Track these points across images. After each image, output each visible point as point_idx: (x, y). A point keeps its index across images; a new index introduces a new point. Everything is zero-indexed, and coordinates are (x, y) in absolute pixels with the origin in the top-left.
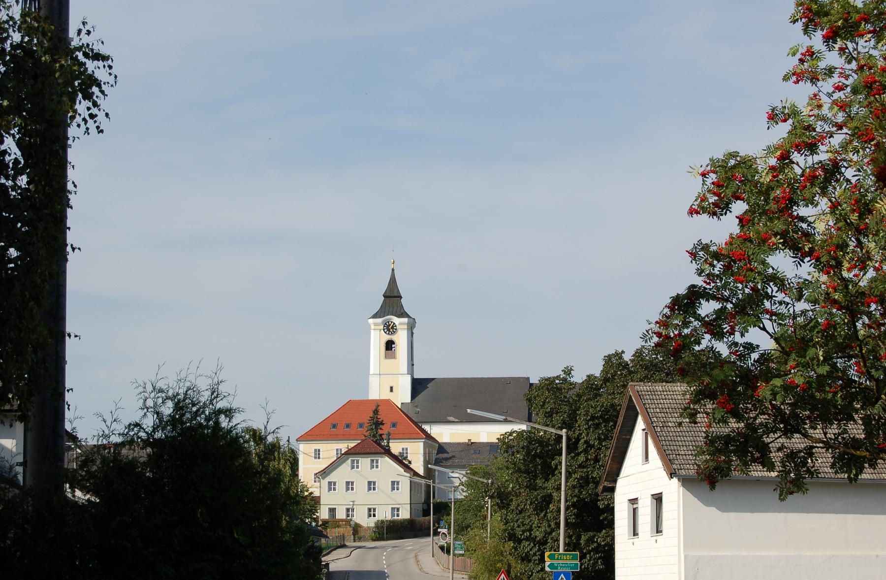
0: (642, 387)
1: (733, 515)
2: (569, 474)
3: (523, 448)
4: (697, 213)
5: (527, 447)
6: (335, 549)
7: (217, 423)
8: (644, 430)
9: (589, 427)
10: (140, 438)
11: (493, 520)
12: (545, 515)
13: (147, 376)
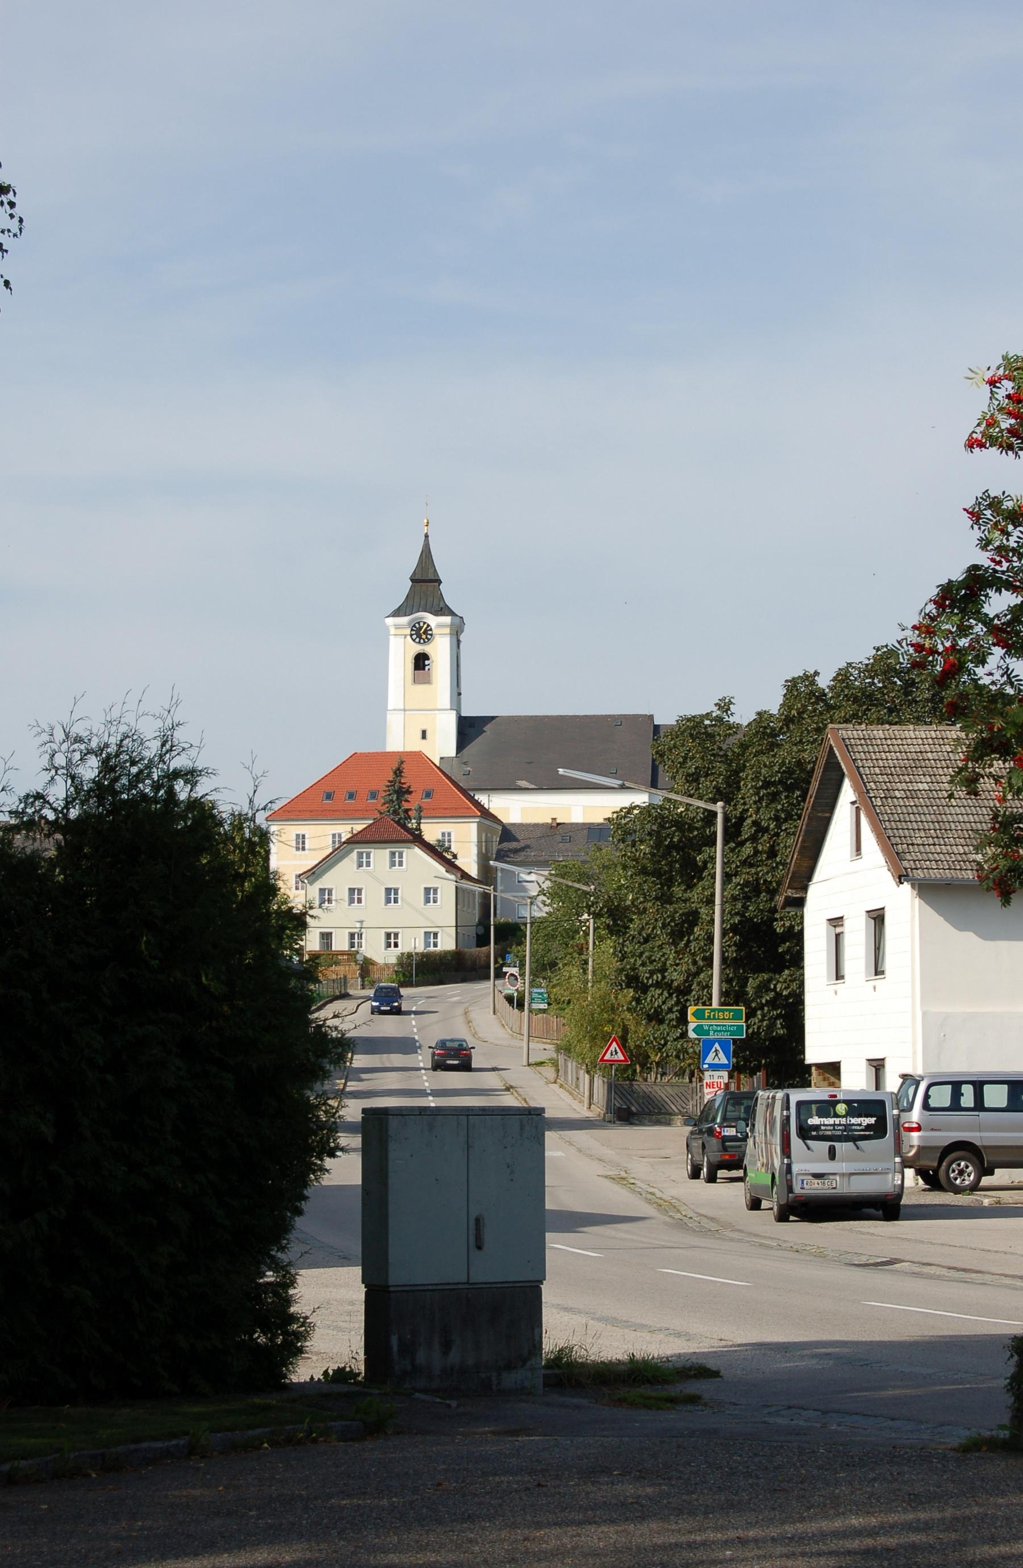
0: (851, 732)
1: (1003, 945)
2: (727, 877)
3: (649, 834)
4: (982, 445)
5: (658, 832)
6: (331, 1001)
7: (171, 793)
8: (853, 803)
9: (761, 799)
10: (45, 818)
11: (600, 953)
12: (687, 945)
13: (56, 715)
